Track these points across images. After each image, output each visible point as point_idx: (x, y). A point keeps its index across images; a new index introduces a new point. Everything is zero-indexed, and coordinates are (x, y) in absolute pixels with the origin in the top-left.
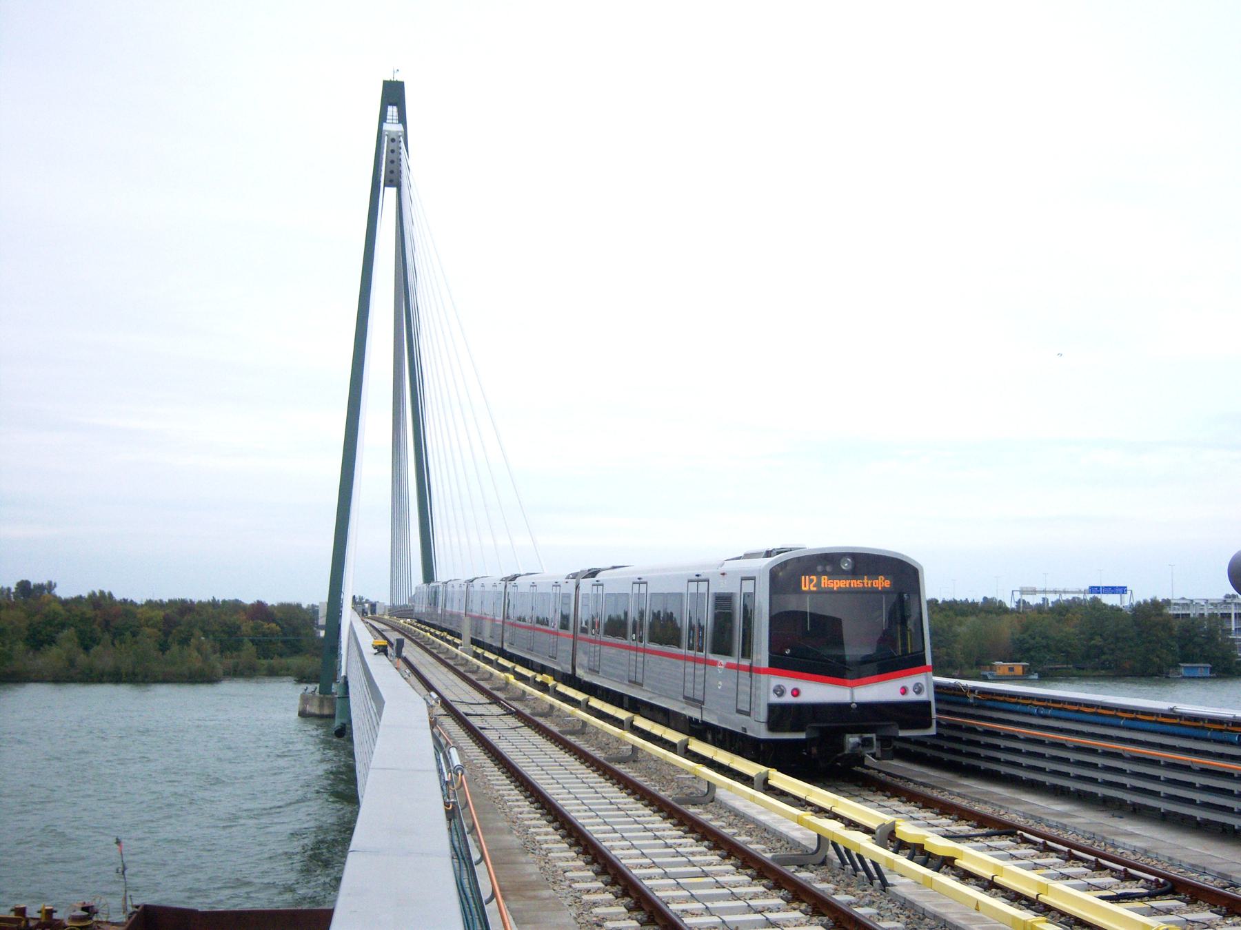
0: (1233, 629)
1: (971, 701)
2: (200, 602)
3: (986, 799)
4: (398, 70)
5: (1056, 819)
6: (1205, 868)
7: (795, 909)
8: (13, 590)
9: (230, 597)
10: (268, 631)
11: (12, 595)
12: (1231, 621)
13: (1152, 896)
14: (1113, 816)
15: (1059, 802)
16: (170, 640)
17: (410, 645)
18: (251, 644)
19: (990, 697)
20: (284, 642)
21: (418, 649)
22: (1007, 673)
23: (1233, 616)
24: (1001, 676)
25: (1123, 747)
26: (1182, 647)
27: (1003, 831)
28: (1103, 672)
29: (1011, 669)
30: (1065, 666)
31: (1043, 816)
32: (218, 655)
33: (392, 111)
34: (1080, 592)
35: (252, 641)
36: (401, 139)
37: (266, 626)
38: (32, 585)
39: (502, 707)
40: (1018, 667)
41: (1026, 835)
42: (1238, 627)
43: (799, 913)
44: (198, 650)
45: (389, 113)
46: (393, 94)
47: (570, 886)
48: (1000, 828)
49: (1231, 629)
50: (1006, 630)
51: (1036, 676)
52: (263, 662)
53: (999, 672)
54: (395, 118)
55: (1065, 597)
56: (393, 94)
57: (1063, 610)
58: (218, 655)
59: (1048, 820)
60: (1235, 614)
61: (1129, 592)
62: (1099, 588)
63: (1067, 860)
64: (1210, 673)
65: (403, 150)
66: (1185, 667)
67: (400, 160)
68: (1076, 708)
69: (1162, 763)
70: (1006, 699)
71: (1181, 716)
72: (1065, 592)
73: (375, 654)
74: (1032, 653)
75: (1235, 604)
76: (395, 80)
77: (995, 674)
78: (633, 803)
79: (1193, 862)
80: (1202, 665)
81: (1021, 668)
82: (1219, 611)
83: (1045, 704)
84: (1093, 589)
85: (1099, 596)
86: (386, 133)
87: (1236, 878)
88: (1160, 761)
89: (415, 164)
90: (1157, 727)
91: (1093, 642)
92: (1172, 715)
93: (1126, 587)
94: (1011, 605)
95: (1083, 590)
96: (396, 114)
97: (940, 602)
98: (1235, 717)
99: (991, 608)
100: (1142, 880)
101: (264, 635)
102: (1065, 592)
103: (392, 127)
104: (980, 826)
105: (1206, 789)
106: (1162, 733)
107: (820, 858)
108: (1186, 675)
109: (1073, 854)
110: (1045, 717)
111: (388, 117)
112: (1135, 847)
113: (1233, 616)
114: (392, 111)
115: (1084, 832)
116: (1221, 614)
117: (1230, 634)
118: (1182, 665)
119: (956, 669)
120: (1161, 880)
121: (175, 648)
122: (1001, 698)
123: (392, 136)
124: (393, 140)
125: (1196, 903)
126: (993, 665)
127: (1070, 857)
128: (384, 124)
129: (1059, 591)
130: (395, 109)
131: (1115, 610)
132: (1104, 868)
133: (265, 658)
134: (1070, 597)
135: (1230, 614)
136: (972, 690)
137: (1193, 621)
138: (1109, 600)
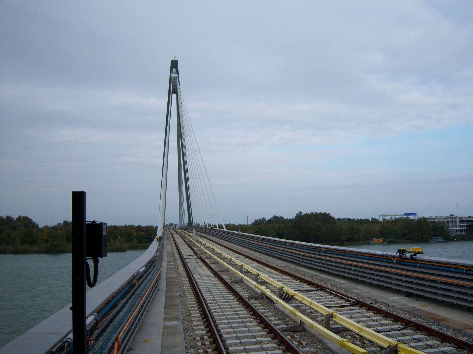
0: (450, 226)
1: (323, 251)
2: (316, 213)
3: (323, 280)
4: (176, 57)
5: (339, 285)
6: (371, 298)
7: (246, 311)
8: (62, 224)
9: (131, 224)
10: (141, 235)
11: (62, 226)
12: (449, 223)
13: (351, 306)
14: (356, 284)
15: (343, 280)
16: (111, 238)
17: (179, 238)
18: (136, 239)
19: (328, 250)
20: (147, 238)
21: (181, 239)
22: (377, 242)
23: (450, 221)
24: (375, 243)
25: (358, 264)
26: (434, 232)
27: (321, 289)
28: (408, 241)
29: (378, 241)
30: (396, 239)
31: (336, 285)
32: (126, 243)
33: (174, 70)
34: (401, 215)
35: (136, 238)
36: (177, 78)
37: (141, 233)
38: (68, 222)
39: (198, 256)
40: (381, 240)
41: (327, 290)
42: (452, 225)
43: (390, 321)
44: (120, 241)
45: (173, 70)
46: (174, 64)
47: (188, 306)
48: (321, 288)
49: (449, 226)
50: (377, 228)
51: (386, 243)
52: (140, 244)
53: (374, 242)
54: (175, 72)
55: (397, 217)
56: (174, 64)
57: (396, 221)
58: (126, 243)
59: (337, 286)
60: (451, 221)
61: (417, 215)
62: (407, 214)
63: (335, 297)
64: (443, 240)
65: (178, 82)
66: (435, 239)
67: (177, 85)
68: (348, 252)
69: (367, 268)
70: (332, 250)
71: (372, 254)
72: (396, 215)
73: (157, 241)
74: (385, 236)
75: (451, 218)
76: (175, 60)
77: (373, 242)
78: (302, 284)
79: (369, 296)
80: (440, 238)
81: (381, 240)
82: (446, 220)
83: (341, 251)
84: (405, 214)
85: (409, 216)
86: (172, 77)
87: (378, 300)
88: (366, 268)
89: (182, 88)
90: (368, 258)
91: (405, 231)
92: (370, 254)
93: (416, 213)
94: (381, 220)
95: (402, 215)
96: (175, 70)
97: (356, 220)
98: (384, 254)
99: (374, 221)
100: (351, 302)
101: (141, 236)
102: (396, 215)
103: (174, 75)
104: (317, 287)
105: (377, 275)
106: (371, 260)
107: (261, 297)
108: (435, 241)
109: (337, 295)
110: (341, 255)
111: (173, 72)
112: (356, 292)
113: (450, 221)
114: (174, 70)
115: (345, 289)
116: (446, 221)
117: (449, 228)
118: (433, 238)
119: (361, 241)
120: (355, 301)
121: (112, 241)
122: (331, 250)
123: (174, 78)
124: (175, 79)
125: (362, 307)
126: (373, 240)
127: (336, 296)
128: (172, 74)
129: (394, 215)
130: (175, 69)
131: (413, 220)
132: (343, 298)
133: (140, 243)
134: (400, 217)
135: (449, 221)
136: (324, 248)
137: (437, 224)
138: (412, 217)
